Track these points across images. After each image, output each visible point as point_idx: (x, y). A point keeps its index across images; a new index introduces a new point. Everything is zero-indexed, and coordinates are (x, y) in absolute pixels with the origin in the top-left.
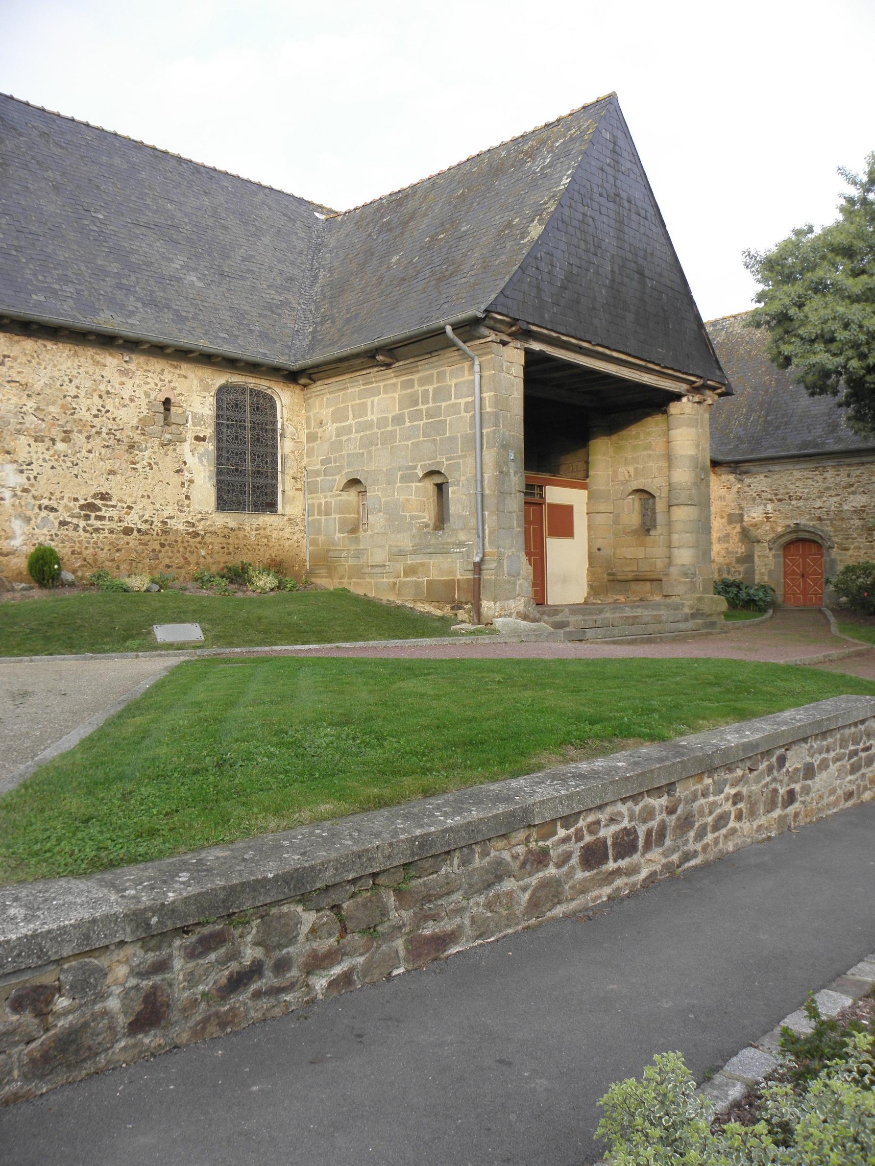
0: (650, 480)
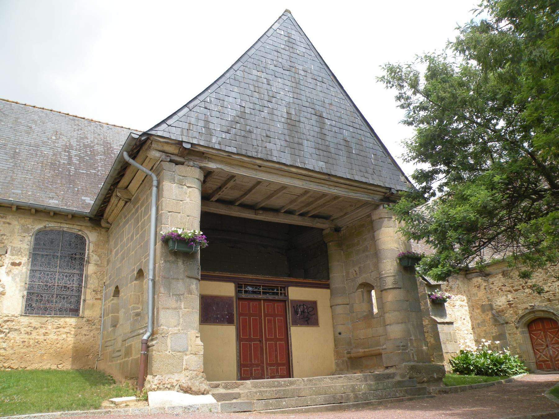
0: (369, 274)
